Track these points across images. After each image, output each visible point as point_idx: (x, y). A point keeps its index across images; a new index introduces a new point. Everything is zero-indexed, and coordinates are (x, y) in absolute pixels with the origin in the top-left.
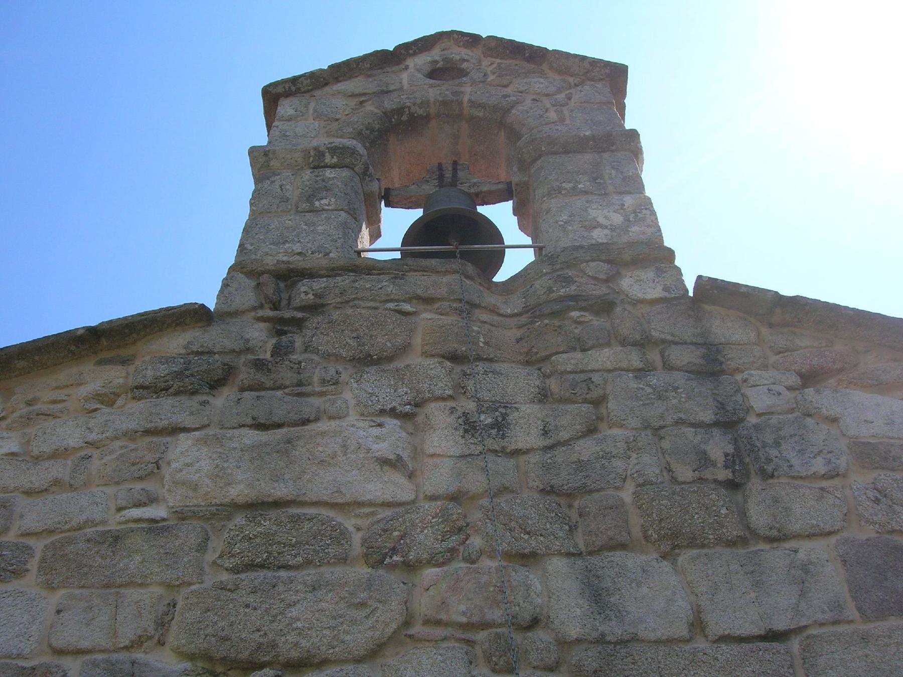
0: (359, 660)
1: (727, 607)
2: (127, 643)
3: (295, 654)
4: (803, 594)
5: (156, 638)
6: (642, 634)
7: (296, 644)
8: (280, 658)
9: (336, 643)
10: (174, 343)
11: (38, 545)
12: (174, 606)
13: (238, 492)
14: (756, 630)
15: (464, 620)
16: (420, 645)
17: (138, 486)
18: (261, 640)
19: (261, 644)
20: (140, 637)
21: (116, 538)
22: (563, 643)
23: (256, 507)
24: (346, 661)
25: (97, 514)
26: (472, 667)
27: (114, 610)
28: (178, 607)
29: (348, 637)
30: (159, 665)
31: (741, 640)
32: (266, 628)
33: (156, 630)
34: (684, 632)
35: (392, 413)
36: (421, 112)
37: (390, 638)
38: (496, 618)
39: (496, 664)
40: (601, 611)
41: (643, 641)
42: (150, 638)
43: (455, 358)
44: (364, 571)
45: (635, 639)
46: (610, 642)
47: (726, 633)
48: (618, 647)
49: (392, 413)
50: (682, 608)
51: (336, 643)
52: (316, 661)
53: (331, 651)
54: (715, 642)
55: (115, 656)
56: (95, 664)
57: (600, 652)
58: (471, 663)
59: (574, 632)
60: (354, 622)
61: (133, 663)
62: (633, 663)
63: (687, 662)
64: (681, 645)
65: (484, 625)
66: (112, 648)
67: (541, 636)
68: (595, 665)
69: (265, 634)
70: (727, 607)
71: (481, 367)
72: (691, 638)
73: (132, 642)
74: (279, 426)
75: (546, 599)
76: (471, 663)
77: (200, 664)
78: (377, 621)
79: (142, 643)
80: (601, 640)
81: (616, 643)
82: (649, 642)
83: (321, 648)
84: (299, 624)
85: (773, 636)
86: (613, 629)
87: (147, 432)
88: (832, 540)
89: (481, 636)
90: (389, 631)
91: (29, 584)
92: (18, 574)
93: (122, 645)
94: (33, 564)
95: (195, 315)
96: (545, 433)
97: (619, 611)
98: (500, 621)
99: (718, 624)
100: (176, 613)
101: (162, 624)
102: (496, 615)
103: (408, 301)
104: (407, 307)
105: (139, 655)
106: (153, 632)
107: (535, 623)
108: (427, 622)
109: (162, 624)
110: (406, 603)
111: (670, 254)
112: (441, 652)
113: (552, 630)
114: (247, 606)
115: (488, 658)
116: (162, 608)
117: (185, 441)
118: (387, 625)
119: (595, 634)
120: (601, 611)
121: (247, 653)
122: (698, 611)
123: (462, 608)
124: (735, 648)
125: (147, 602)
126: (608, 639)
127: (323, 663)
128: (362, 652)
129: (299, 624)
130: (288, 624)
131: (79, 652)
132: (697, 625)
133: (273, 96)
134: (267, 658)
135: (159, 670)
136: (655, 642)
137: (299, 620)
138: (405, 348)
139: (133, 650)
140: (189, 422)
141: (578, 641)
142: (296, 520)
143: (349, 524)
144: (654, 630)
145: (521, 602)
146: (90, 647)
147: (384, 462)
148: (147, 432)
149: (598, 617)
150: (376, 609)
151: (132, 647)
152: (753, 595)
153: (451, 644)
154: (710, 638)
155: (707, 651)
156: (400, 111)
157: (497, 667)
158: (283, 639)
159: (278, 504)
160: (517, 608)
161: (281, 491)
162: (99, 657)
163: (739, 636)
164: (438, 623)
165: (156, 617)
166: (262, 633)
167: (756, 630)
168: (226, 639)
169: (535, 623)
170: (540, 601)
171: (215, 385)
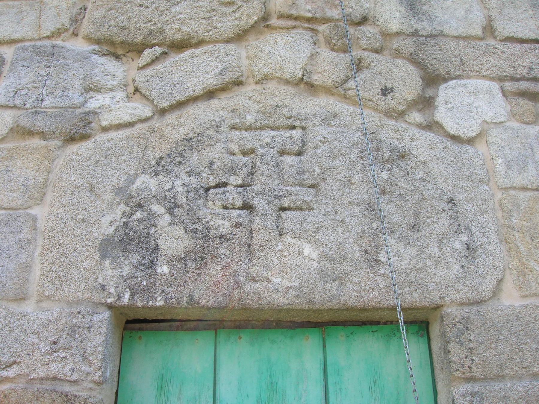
0: (228, 41)
1: (512, 18)
2: (49, 33)
3: (178, 36)
5: (71, 31)
6: (446, 32)
7: (179, 30)
8: (167, 40)
9: (210, 28)
12: (85, 10)
14: (534, 35)
15: (309, 15)
16: (274, 32)
18: (152, 28)
19: (151, 30)
20: (59, 29)
22: (386, 35)
24: (218, 42)
26: (316, 46)
27: (38, 13)
28: (88, 10)
29: (220, 25)
30: (73, 48)
31: (522, 41)
32: (156, 20)
33: (71, 25)
34: (479, 32)
37: (252, 27)
38: (334, 15)
39: (335, 45)
40: (415, 15)
41: (447, 36)
42: (67, 30)
45: (441, 34)
46: (422, 36)
47: (511, 35)
48: (429, 39)
50: (478, 17)
51: (210, 28)
52: (194, 41)
53: (207, 34)
54: (502, 41)
55: (39, 43)
56: (25, 49)
57: (415, 42)
58: (315, 44)
59: (394, 27)
60: (224, 15)
61: (53, 47)
62: (440, 50)
63: (481, 52)
64: (476, 41)
65: (325, 20)
66: (38, 38)
67: (368, 29)
68: (411, 50)
69: (155, 24)
70: (512, 18)
72: (484, 37)
73: (53, 33)
75: (373, 5)
76: (315, 44)
77: (105, 48)
78: (242, 14)
79: (60, 34)
80: (415, 34)
81: (427, 37)
82: (452, 37)
83: (199, 32)
84: (181, 16)
86: (425, 27)
89: (322, 28)
90: (251, 22)
93: (45, 35)
97: (429, 16)
98: (337, 17)
99: (506, 28)
100: (86, 14)
101: (76, 21)
102: (335, 13)
105: (58, 42)
106: (69, 26)
107: (364, 20)
108: (281, 16)
109: (76, 21)
110: (264, 3)
112: (292, 35)
113: (378, 25)
114: (141, 6)
115: (328, 41)
116: (75, 11)
118: (250, 17)
119: (410, 30)
120: (415, 15)
121: (141, 37)
122: (490, 19)
123: (309, 7)
124: (518, 46)
125: (64, 6)
126: (420, 33)
127: (200, 43)
128: (231, 35)
129: (181, 16)
130: (173, 17)
131: (12, 42)
132: (489, 29)
134: (156, 41)
135: (74, 50)
136: (456, 37)
137: (181, 14)
139: (54, 39)
141: (398, 34)
144: (456, 29)
145: (354, 6)
146: (20, 38)
149: (413, 19)
150: (241, 6)
151: (53, 36)
152: (531, 13)
153: (300, 31)
154: (498, 38)
155: (497, 46)
157: (335, 47)
158: (169, 27)
160: (351, 10)
162: (28, 44)
163: (521, 38)
164: (289, 17)
165: (71, 16)
166: (152, 23)
167: (534, 35)
168: (124, 28)
169: (364, 20)
170: (368, 5)
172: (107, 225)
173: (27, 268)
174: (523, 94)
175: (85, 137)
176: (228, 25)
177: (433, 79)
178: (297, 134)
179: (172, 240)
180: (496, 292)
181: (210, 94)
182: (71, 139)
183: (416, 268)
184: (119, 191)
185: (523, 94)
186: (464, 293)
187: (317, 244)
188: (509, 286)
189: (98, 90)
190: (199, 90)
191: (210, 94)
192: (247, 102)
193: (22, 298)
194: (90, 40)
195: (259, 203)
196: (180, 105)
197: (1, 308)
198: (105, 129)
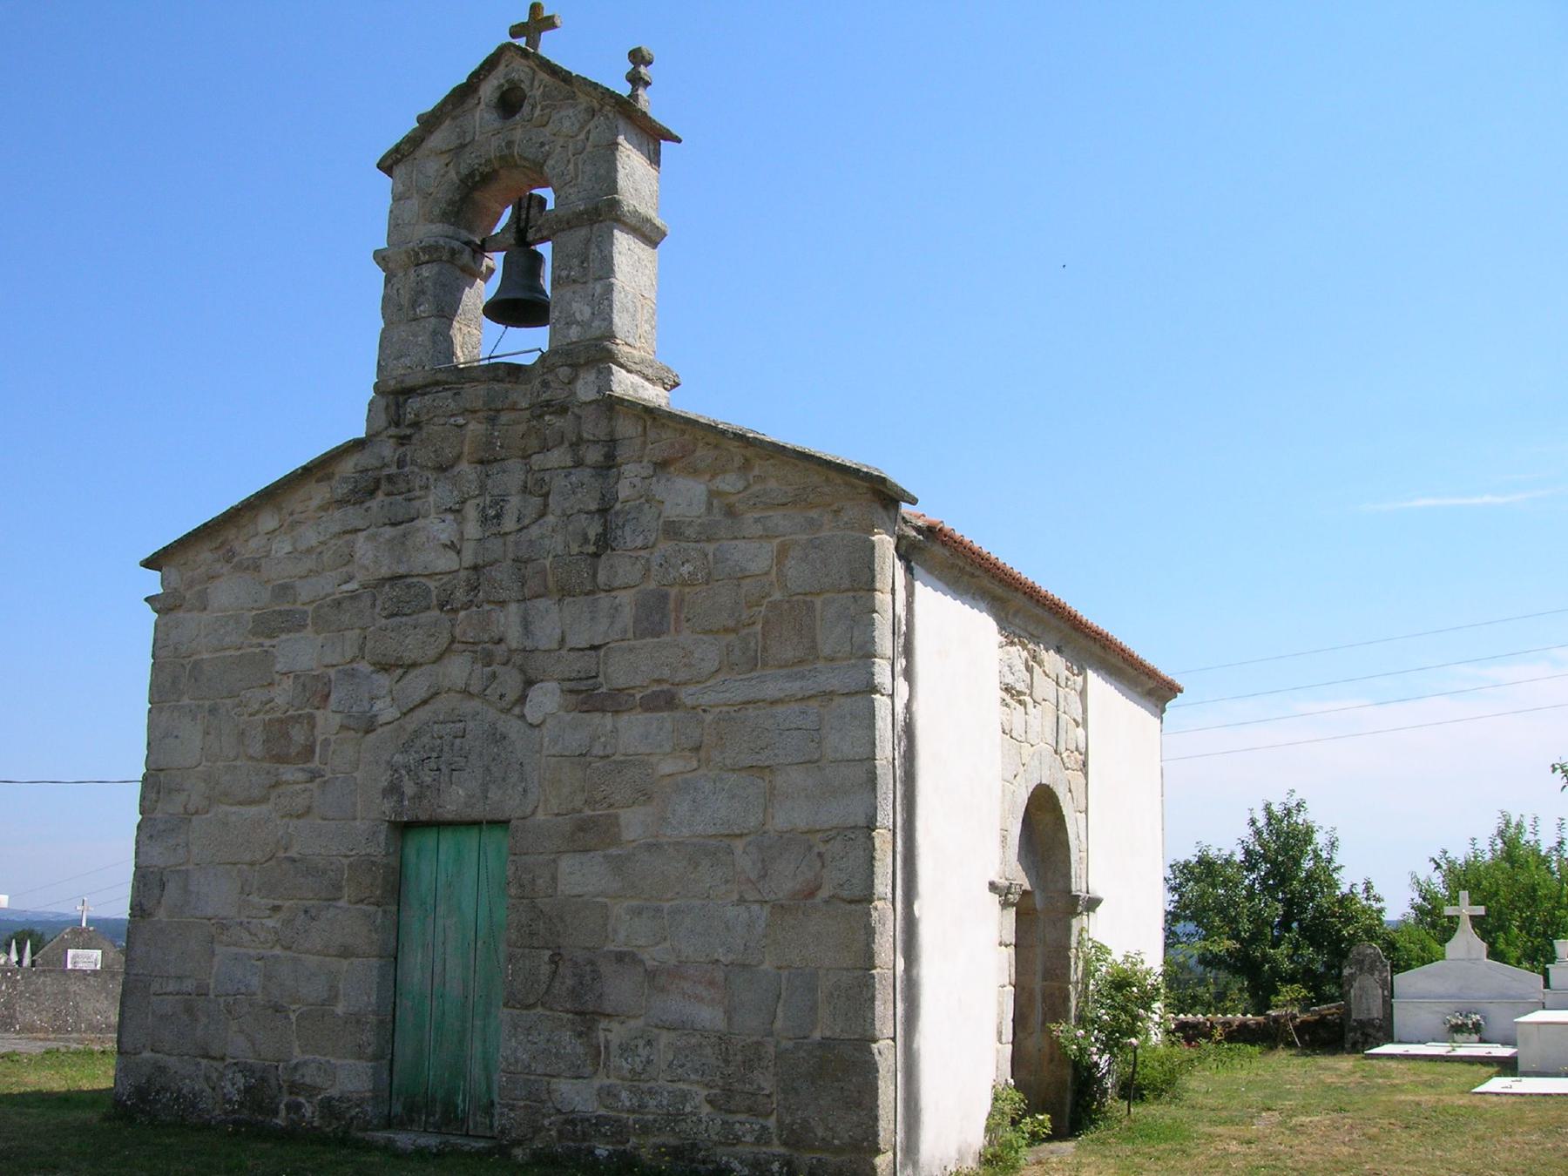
4: (612, 623)
10: (348, 467)
11: (310, 608)
13: (385, 572)
17: (345, 569)
21: (338, 603)
23: (395, 578)
25: (329, 589)
35: (450, 510)
36: (487, 170)
43: (481, 462)
44: (436, 612)
49: (450, 510)
59: (514, 645)
67: (503, 646)
71: (1085, 935)
74: (401, 523)
85: (594, 648)
86: (529, 644)
87: (345, 532)
88: (633, 591)
91: (309, 631)
92: (305, 626)
94: (309, 621)
95: (357, 445)
96: (519, 520)
99: (573, 641)
103: (462, 414)
104: (461, 421)
107: (500, 641)
109: (361, 649)
111: (377, 387)
117: (361, 536)
132: (562, 641)
133: (388, 165)
138: (458, 458)
140: (360, 524)
142: (409, 586)
143: (432, 584)
147: (445, 546)
148: (345, 532)
156: (471, 175)
159: (401, 577)
161: (402, 570)
169: (500, 641)
171: (372, 493)
172: (384, 782)
173: (355, 804)
174: (571, 691)
176: (432, 652)
177: (529, 683)
178: (461, 725)
179: (409, 788)
180: (533, 813)
181: (425, 702)
182: (367, 732)
183: (504, 801)
184: (388, 763)
186: (519, 814)
188: (540, 810)
190: (418, 701)
191: (425, 702)
192: (441, 705)
193: (355, 819)
195: (443, 767)
196: (412, 710)
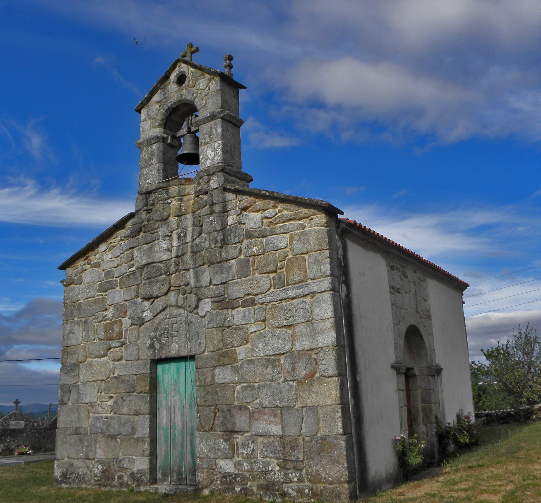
34: (208, 285)
47: (149, 104)
99: (214, 282)
175: (143, 324)
185: (215, 302)
187: (177, 344)
189: (144, 311)
191: (161, 311)
194: (142, 298)
195: (169, 336)
197: (1, 489)
198: (146, 322)
